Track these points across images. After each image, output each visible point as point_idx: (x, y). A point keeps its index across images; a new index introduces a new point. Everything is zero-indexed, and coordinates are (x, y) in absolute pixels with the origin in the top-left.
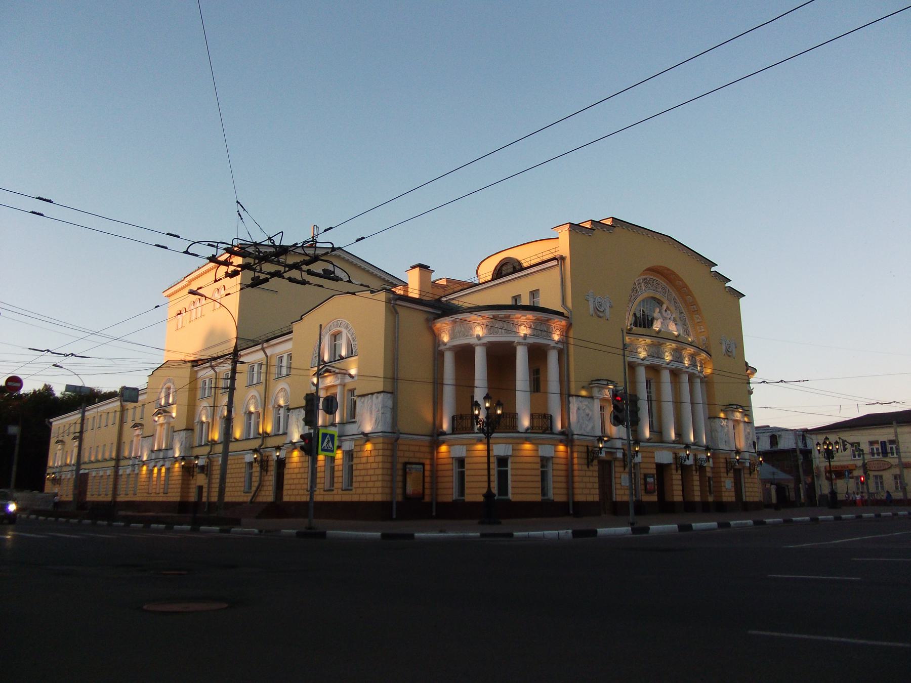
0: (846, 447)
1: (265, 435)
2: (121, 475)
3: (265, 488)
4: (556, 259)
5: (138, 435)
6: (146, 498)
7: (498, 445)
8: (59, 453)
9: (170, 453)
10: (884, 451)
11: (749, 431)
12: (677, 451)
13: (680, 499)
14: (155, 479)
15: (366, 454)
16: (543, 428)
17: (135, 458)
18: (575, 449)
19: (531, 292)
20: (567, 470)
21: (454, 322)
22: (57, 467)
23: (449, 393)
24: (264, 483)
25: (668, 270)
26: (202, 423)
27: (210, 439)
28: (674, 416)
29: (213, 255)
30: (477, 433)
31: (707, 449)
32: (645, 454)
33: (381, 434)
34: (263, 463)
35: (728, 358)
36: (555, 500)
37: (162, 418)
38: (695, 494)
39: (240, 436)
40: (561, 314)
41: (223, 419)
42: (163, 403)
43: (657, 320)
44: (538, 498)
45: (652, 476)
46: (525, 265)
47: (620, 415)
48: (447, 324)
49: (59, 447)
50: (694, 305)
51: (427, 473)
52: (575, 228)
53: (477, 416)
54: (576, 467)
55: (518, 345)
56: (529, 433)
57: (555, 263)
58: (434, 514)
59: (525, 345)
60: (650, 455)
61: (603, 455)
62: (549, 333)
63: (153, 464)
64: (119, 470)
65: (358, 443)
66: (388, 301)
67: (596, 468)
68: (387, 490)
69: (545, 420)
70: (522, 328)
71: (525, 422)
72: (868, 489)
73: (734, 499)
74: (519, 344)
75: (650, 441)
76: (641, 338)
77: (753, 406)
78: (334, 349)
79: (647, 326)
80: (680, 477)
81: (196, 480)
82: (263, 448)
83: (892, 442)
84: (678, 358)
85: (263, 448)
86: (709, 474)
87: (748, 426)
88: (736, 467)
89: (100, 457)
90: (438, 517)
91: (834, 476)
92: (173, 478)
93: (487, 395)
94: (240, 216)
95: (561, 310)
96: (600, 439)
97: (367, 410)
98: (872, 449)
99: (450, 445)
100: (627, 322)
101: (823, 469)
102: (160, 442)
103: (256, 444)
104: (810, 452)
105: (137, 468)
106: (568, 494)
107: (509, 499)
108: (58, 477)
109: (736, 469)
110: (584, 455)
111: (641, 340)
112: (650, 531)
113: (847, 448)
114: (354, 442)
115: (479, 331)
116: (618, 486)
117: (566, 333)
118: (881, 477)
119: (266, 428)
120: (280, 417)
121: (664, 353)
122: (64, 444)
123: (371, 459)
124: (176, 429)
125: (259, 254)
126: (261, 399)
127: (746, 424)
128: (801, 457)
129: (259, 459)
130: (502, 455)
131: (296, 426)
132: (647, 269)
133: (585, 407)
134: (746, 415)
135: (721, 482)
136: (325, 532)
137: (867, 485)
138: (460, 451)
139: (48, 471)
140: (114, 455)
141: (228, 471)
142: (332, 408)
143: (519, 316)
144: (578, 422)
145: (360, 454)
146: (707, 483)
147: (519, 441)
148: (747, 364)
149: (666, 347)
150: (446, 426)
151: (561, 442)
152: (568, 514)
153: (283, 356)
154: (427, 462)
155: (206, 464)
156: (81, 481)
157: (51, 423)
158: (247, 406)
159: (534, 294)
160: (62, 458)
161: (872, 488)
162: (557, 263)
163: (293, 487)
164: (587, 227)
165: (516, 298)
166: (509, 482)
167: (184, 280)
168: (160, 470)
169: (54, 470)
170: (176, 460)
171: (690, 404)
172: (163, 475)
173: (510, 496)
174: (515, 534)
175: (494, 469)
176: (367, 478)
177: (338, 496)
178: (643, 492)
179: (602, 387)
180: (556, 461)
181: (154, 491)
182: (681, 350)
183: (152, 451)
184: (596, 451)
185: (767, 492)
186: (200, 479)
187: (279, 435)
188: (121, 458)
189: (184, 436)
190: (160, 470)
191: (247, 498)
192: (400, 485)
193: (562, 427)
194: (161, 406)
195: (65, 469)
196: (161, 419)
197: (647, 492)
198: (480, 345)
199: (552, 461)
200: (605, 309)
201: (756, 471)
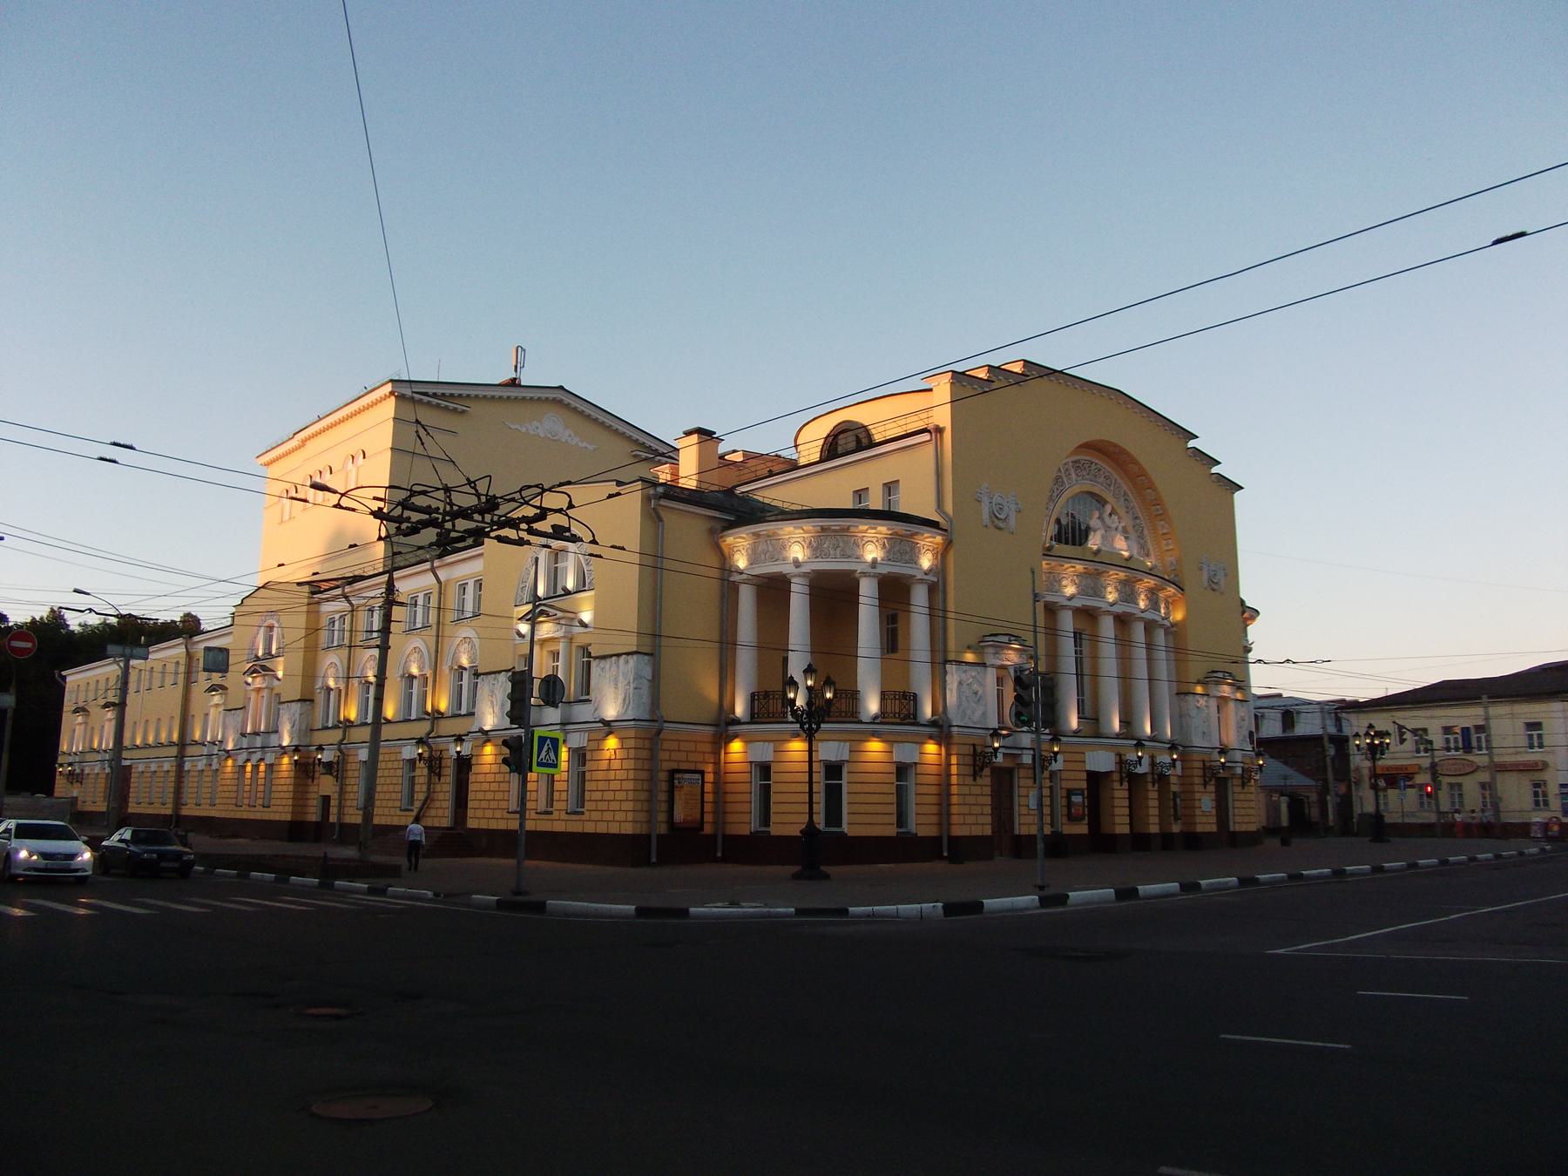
0: (1404, 737)
1: (436, 715)
2: (189, 771)
3: (437, 804)
4: (929, 431)
5: (217, 705)
6: (233, 813)
7: (825, 743)
8: (79, 730)
9: (273, 740)
10: (1466, 744)
11: (1243, 714)
12: (1122, 752)
13: (1126, 830)
15: (607, 755)
16: (902, 716)
18: (954, 750)
19: (885, 484)
20: (940, 814)
21: (757, 535)
23: (745, 661)
26: (329, 689)
27: (342, 718)
29: (379, 508)
30: (792, 722)
31: (1173, 747)
32: (1069, 757)
33: (632, 723)
34: (434, 764)
39: (394, 715)
40: (933, 525)
42: (260, 654)
43: (1095, 531)
44: (892, 831)
45: (1080, 792)
46: (878, 438)
47: (1024, 694)
49: (80, 719)
52: (959, 378)
53: (794, 701)
56: (878, 723)
57: (926, 437)
58: (719, 854)
60: (1078, 757)
61: (1000, 758)
62: (913, 560)
63: (243, 756)
65: (595, 736)
66: (647, 499)
67: (987, 781)
68: (642, 817)
69: (905, 702)
70: (870, 547)
71: (872, 705)
72: (1438, 806)
73: (1214, 828)
74: (864, 574)
75: (1078, 734)
80: (1126, 794)
81: (318, 785)
82: (435, 737)
83: (1480, 729)
84: (1129, 596)
85: (435, 737)
86: (1174, 788)
88: (1220, 775)
89: (151, 740)
90: (725, 860)
91: (1382, 783)
92: (278, 782)
93: (810, 665)
95: (935, 517)
96: (995, 734)
101: (1366, 772)
103: (421, 729)
104: (1345, 740)
105: (215, 761)
106: (940, 824)
108: (78, 771)
109: (1219, 780)
110: (969, 760)
111: (1066, 566)
113: (1405, 740)
114: (586, 735)
116: (1024, 810)
117: (943, 554)
118: (1460, 785)
119: (438, 703)
120: (461, 685)
123: (616, 765)
125: (451, 508)
128: (1331, 751)
129: (426, 755)
132: (1083, 444)
134: (1239, 688)
136: (544, 903)
137: (1437, 799)
138: (764, 753)
139: (61, 759)
140: (175, 737)
143: (866, 527)
145: (597, 755)
146: (1172, 810)
147: (856, 737)
148: (1242, 602)
150: (740, 710)
155: (336, 758)
156: (120, 778)
157: (64, 678)
160: (84, 739)
161: (1445, 805)
163: (484, 804)
164: (980, 376)
165: (860, 494)
167: (293, 437)
169: (71, 759)
170: (284, 750)
171: (1147, 681)
172: (262, 775)
173: (845, 828)
174: (851, 909)
176: (610, 796)
177: (560, 824)
178: (1065, 820)
179: (1000, 647)
183: (243, 735)
185: (1273, 809)
186: (327, 785)
187: (460, 715)
189: (298, 711)
190: (256, 767)
192: (664, 807)
193: (933, 714)
194: (258, 659)
195: (89, 757)
197: (1071, 818)
198: (799, 576)
199: (916, 769)
200: (1008, 515)
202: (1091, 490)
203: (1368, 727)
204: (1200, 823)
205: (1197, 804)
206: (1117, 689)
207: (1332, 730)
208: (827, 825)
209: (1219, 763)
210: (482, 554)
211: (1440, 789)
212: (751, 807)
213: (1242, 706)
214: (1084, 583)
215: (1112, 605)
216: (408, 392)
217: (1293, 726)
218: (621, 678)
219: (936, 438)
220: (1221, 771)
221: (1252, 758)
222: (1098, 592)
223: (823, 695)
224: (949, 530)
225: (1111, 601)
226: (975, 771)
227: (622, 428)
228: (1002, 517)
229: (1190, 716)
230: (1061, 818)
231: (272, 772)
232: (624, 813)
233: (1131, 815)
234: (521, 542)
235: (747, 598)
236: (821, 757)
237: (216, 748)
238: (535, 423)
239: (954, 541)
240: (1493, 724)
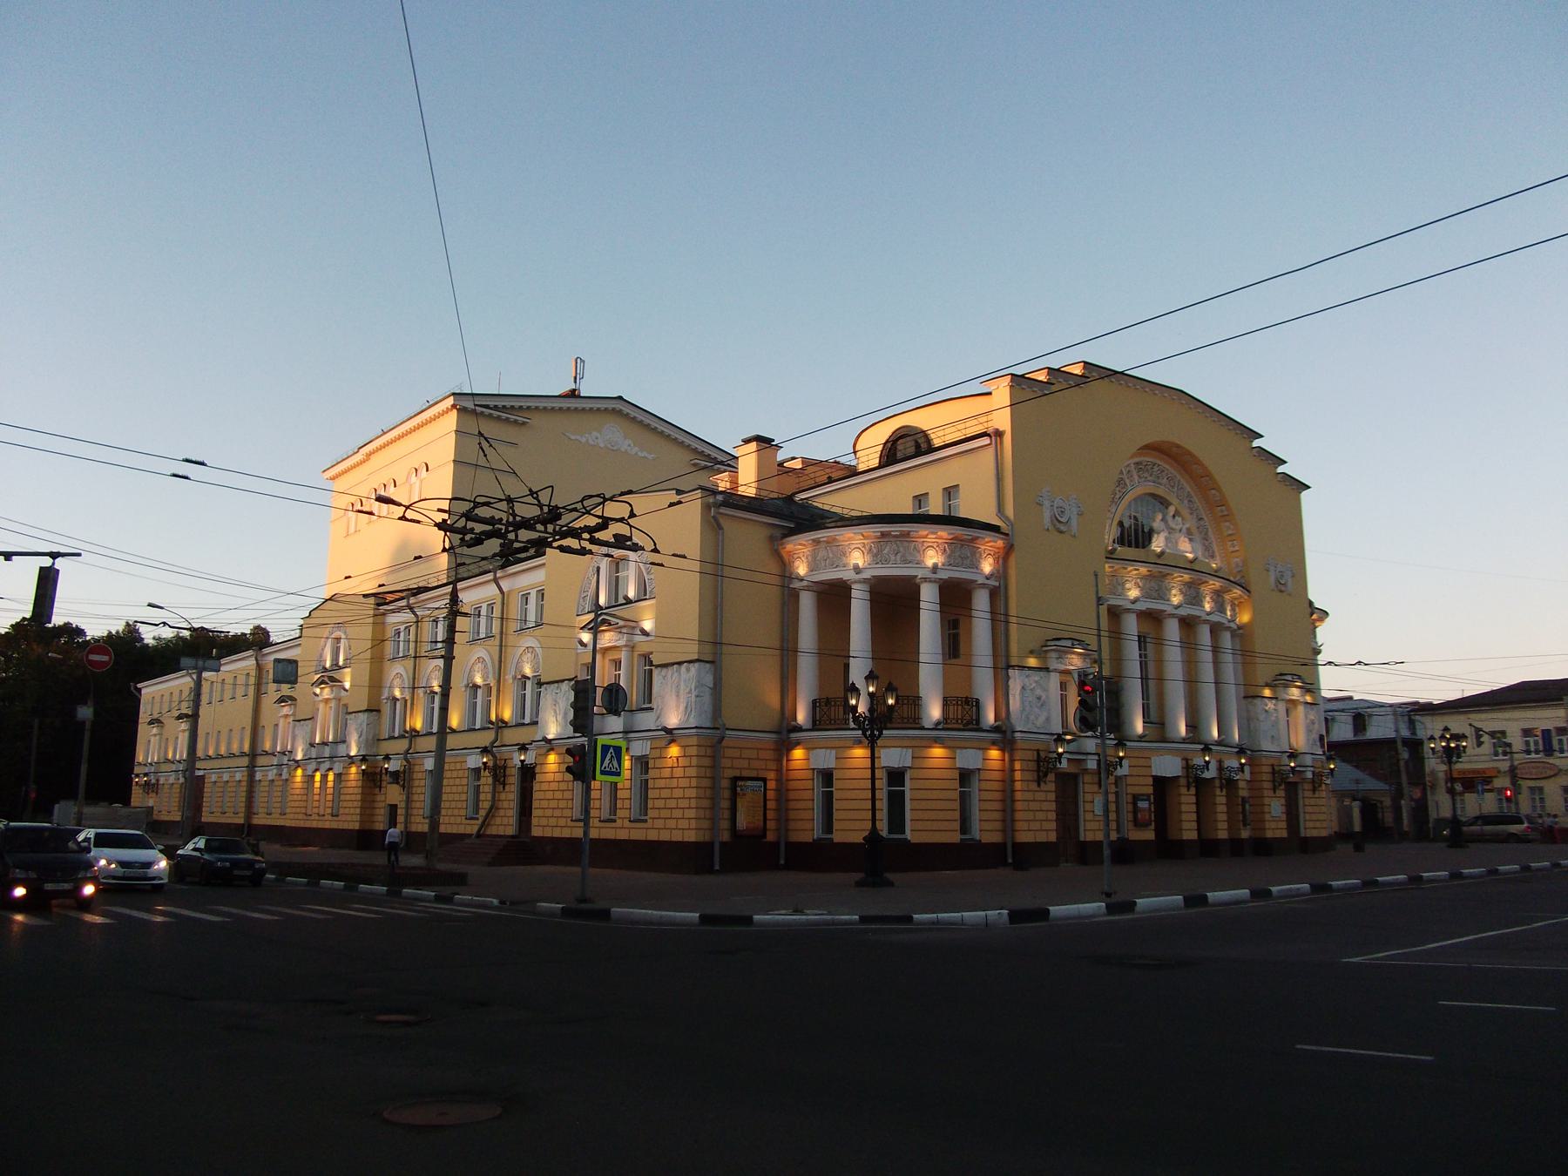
0: (1482, 740)
1: (500, 724)
3: (502, 812)
4: (989, 435)
6: (302, 822)
9: (342, 749)
13: (1193, 835)
14: (317, 791)
15: (670, 763)
17: (283, 753)
18: (1018, 755)
19: (945, 489)
21: (817, 542)
22: (151, 764)
23: (807, 668)
24: (500, 805)
25: (1178, 446)
26: (395, 699)
28: (1186, 708)
31: (1241, 751)
32: (1134, 762)
33: (694, 730)
34: (498, 772)
35: (1280, 594)
36: (983, 841)
37: (327, 691)
38: (1219, 819)
39: (458, 725)
41: (429, 694)
42: (328, 665)
43: (1158, 533)
44: (955, 838)
46: (937, 442)
48: (804, 545)
49: (155, 731)
50: (1223, 505)
51: (771, 795)
52: (1019, 381)
53: (855, 708)
54: (1018, 785)
55: (922, 582)
57: (985, 441)
58: (717, 867)
59: (935, 582)
60: (1141, 762)
61: (1064, 764)
62: (975, 566)
63: (313, 766)
64: (256, 772)
65: (658, 744)
66: (706, 508)
67: (1052, 787)
70: (931, 552)
73: (1284, 834)
74: (925, 580)
76: (1133, 566)
77: (1322, 688)
78: (615, 585)
79: (1141, 544)
84: (1194, 598)
86: (1243, 793)
87: (1312, 709)
88: (1290, 780)
89: (223, 751)
90: (788, 867)
91: (1458, 787)
92: (346, 791)
94: (483, 451)
95: (996, 521)
96: (1059, 739)
97: (671, 691)
98: (1527, 743)
99: (808, 749)
100: (1107, 537)
101: (1441, 776)
102: (324, 730)
103: (486, 738)
105: (285, 770)
106: (1004, 831)
107: (906, 839)
108: (153, 781)
109: (1289, 784)
110: (1033, 766)
111: (1130, 568)
112: (1138, 908)
113: (1483, 743)
115: (857, 558)
116: (1089, 816)
118: (1541, 789)
119: (502, 715)
120: (525, 694)
121: (1170, 590)
122: (162, 727)
123: (678, 772)
124: (350, 710)
125: (514, 518)
126: (493, 662)
127: (1309, 706)
128: (1405, 755)
129: (491, 764)
130: (896, 766)
131: (552, 712)
133: (1034, 685)
134: (1308, 691)
135: (1264, 821)
136: (610, 910)
137: (1517, 804)
138: (825, 759)
139: (137, 770)
140: (246, 748)
141: (444, 797)
142: (617, 704)
143: (926, 533)
144: (1022, 712)
145: (659, 763)
146: (1240, 807)
147: (914, 743)
148: (1311, 603)
149: (1173, 579)
150: (802, 716)
151: (994, 743)
152: (1004, 863)
153: (529, 593)
154: (771, 775)
155: (403, 768)
157: (139, 690)
158: (470, 676)
159: (950, 493)
162: (989, 442)
163: (549, 813)
164: (1040, 379)
165: (920, 499)
166: (908, 815)
167: (358, 452)
168: (324, 777)
169: (146, 770)
172: (330, 784)
173: (908, 835)
175: (882, 789)
176: (672, 804)
178: (1131, 825)
179: (1063, 652)
180: (984, 775)
181: (316, 810)
182: (1200, 584)
183: (312, 745)
184: (1052, 758)
185: (1345, 814)
186: (393, 794)
188: (259, 751)
190: (324, 777)
191: (472, 828)
192: (727, 814)
194: (325, 670)
195: (164, 767)
196: (326, 693)
197: (1137, 824)
198: (859, 582)
200: (1070, 518)
201: (1323, 785)
207: (1405, 733)
209: (1289, 768)
210: (544, 564)
216: (469, 405)
217: (1365, 729)
221: (1322, 762)
222: (1162, 595)
227: (681, 437)
229: (1258, 720)
233: (1198, 821)
234: (583, 552)
238: (595, 434)
239: (1015, 546)
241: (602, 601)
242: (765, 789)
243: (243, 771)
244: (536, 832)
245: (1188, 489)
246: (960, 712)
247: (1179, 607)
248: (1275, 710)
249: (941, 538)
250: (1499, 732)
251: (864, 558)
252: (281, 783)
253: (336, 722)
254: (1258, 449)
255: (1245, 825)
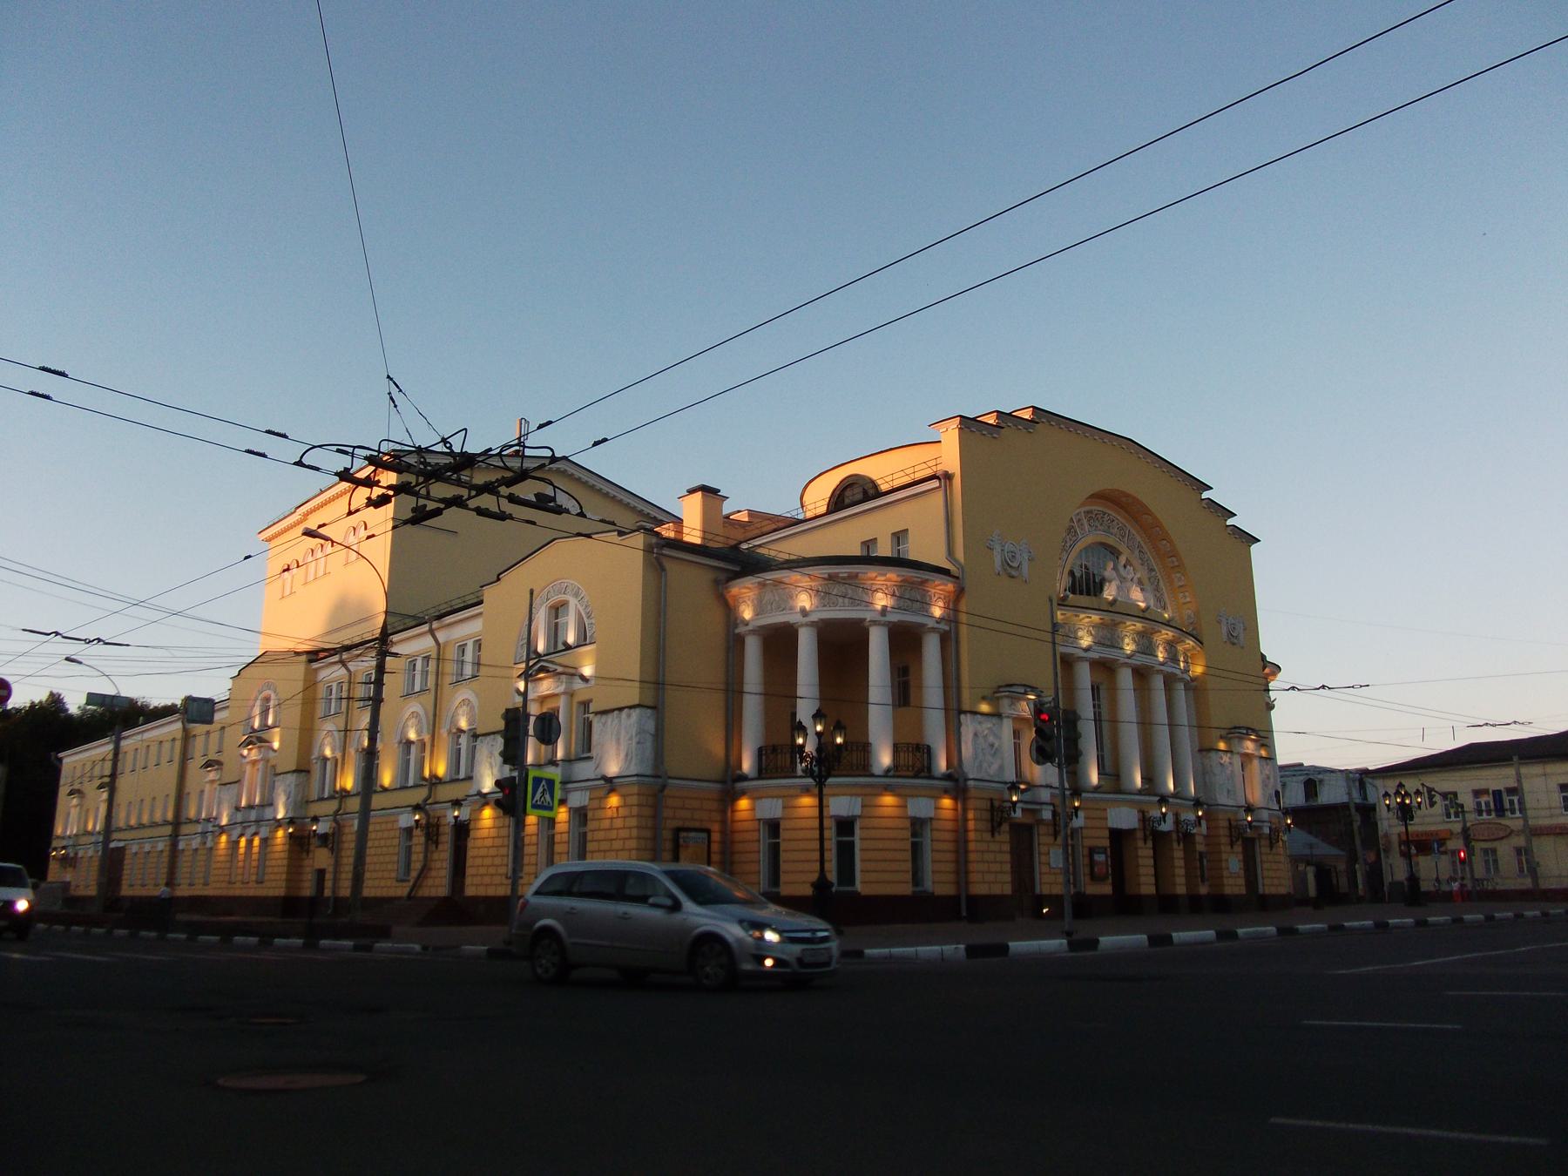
1: (434, 781)
2: (183, 850)
3: (433, 873)
4: (938, 478)
5: (212, 782)
8: (74, 813)
9: (268, 813)
11: (1268, 773)
12: (1145, 808)
13: (1151, 890)
14: (241, 857)
15: (609, 813)
18: (971, 803)
19: (893, 534)
20: (956, 841)
21: (762, 585)
23: (752, 709)
26: (325, 759)
31: (1197, 803)
33: (635, 778)
34: (431, 830)
36: (936, 894)
42: (256, 725)
43: (1110, 582)
44: (906, 889)
45: (1103, 850)
46: (884, 487)
49: (75, 801)
52: (969, 425)
53: (803, 746)
54: (972, 835)
55: (871, 625)
56: (891, 777)
57: (934, 484)
61: (1019, 814)
62: (925, 605)
63: (238, 830)
66: (648, 550)
67: (1006, 837)
69: (918, 754)
73: (1243, 891)
74: (874, 623)
76: (1085, 613)
78: (555, 631)
81: (313, 858)
84: (1147, 648)
86: (1200, 848)
89: (145, 820)
92: (273, 856)
96: (1013, 787)
99: (754, 799)
100: (1058, 585)
101: (1395, 839)
103: (418, 796)
104: (1373, 808)
105: (210, 838)
106: (958, 883)
108: (72, 855)
109: (1247, 840)
110: (987, 815)
111: (1082, 616)
113: (1436, 802)
115: (804, 601)
116: (1045, 869)
118: (1494, 851)
120: (460, 749)
121: (1123, 640)
123: (618, 823)
124: (278, 771)
128: (1357, 819)
129: (424, 822)
133: (986, 732)
134: (1263, 745)
138: (772, 808)
139: (55, 844)
140: (170, 816)
143: (874, 575)
145: (600, 814)
147: (868, 790)
148: (1263, 657)
150: (747, 765)
151: (946, 792)
154: (716, 827)
155: (332, 830)
156: (113, 861)
157: (60, 760)
158: (404, 732)
161: (1479, 871)
165: (868, 544)
166: (858, 866)
167: (295, 512)
169: (64, 843)
170: (278, 824)
171: (1167, 727)
172: (256, 850)
173: (859, 887)
174: (868, 951)
178: (1087, 879)
180: (936, 824)
181: (240, 878)
183: (238, 809)
184: (1005, 807)
185: (1300, 880)
186: (321, 858)
188: (183, 820)
190: (250, 843)
191: (402, 891)
193: (948, 767)
194: (254, 731)
195: (84, 840)
196: (252, 754)
197: (1094, 877)
198: (807, 625)
199: (931, 824)
202: (1103, 541)
203: (1398, 786)
204: (1228, 885)
205: (1224, 865)
206: (1137, 746)
207: (1357, 798)
208: (840, 883)
209: (1246, 823)
210: (481, 614)
211: (1474, 855)
212: (759, 847)
213: (1267, 764)
214: (1101, 634)
215: (1129, 657)
217: (1316, 795)
218: (623, 733)
219: (946, 486)
220: (1248, 830)
221: (1279, 818)
222: (1115, 645)
223: (834, 739)
224: (961, 577)
225: (1129, 652)
226: (993, 827)
227: (627, 499)
228: (1015, 565)
230: (1084, 878)
231: (267, 846)
232: (622, 842)
233: (1156, 875)
234: (502, 516)
235: (753, 649)
236: (832, 813)
237: (211, 825)
239: (966, 589)
240: (1526, 786)
241: (541, 648)
242: (709, 842)
243: (165, 840)
244: (470, 891)
245: (1139, 539)
246: (910, 759)
247: (1133, 656)
248: (1230, 763)
249: (889, 580)
250: (1450, 793)
251: (811, 601)
252: (205, 852)
253: (263, 787)
254: (1207, 501)
255: (1203, 881)
